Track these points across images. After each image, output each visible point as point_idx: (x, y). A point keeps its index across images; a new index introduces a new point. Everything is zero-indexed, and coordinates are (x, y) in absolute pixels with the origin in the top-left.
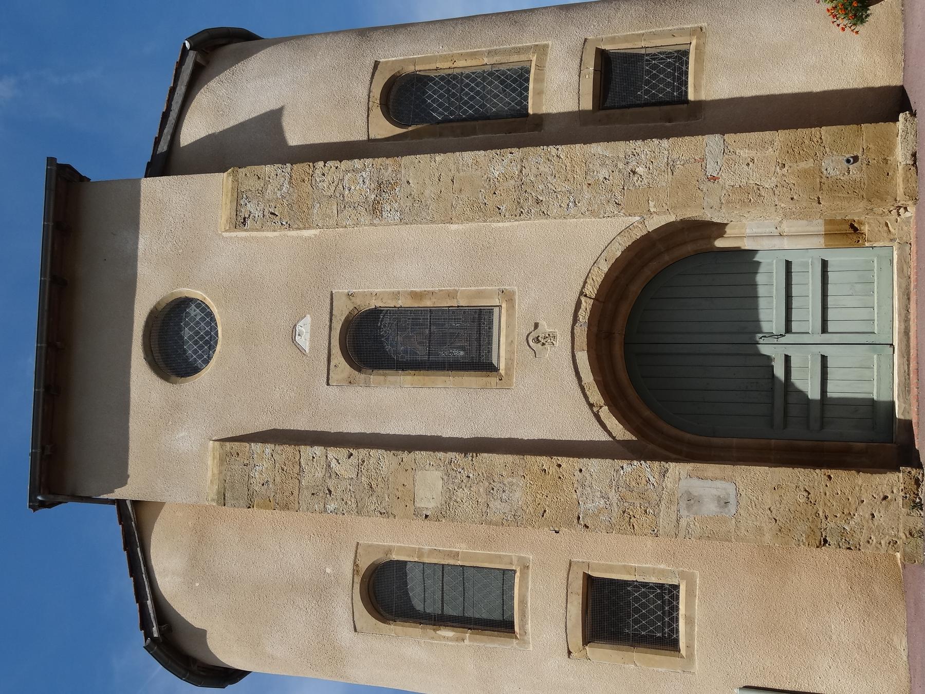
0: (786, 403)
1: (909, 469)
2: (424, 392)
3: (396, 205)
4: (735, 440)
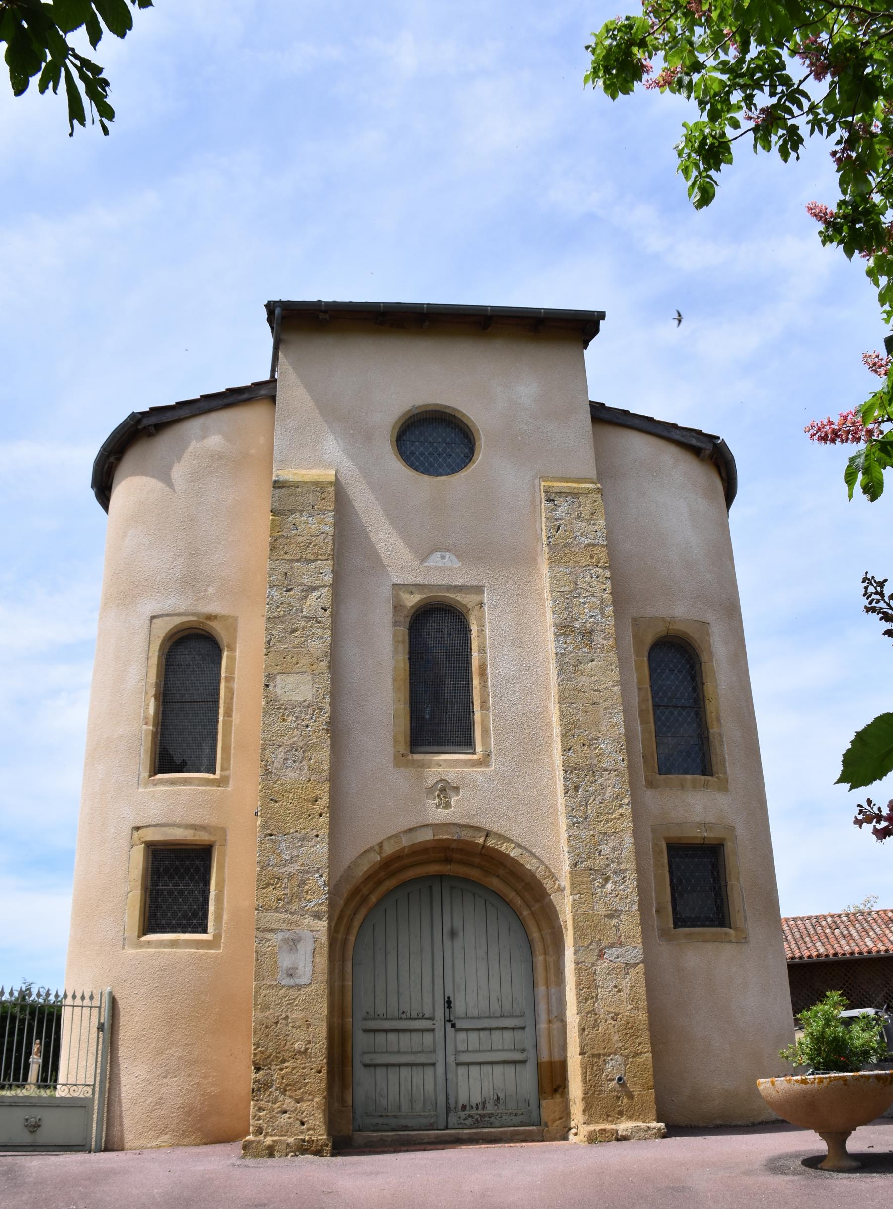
0: (387, 1031)
1: (330, 1144)
2: (389, 682)
3: (570, 648)
4: (350, 983)
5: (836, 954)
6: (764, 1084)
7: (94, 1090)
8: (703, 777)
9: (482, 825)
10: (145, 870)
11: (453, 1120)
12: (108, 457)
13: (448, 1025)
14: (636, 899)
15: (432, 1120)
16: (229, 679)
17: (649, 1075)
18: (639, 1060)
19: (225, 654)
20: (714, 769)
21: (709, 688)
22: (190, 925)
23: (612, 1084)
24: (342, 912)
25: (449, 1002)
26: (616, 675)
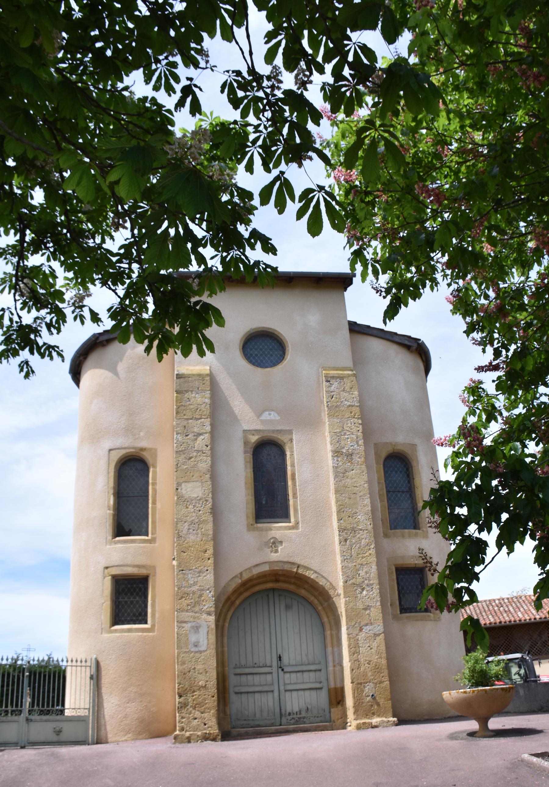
0: (246, 674)
3: (340, 464)
5: (500, 622)
6: (446, 695)
7: (89, 711)
8: (414, 531)
9: (295, 562)
10: (112, 591)
11: (284, 720)
12: (79, 357)
13: (280, 670)
14: (379, 599)
15: (273, 721)
16: (154, 484)
17: (388, 693)
18: (382, 685)
19: (151, 470)
20: (421, 526)
21: (417, 481)
22: (137, 620)
23: (368, 698)
24: (221, 610)
25: (280, 657)
26: (365, 478)
